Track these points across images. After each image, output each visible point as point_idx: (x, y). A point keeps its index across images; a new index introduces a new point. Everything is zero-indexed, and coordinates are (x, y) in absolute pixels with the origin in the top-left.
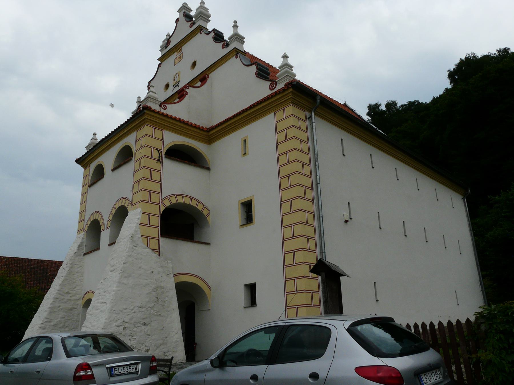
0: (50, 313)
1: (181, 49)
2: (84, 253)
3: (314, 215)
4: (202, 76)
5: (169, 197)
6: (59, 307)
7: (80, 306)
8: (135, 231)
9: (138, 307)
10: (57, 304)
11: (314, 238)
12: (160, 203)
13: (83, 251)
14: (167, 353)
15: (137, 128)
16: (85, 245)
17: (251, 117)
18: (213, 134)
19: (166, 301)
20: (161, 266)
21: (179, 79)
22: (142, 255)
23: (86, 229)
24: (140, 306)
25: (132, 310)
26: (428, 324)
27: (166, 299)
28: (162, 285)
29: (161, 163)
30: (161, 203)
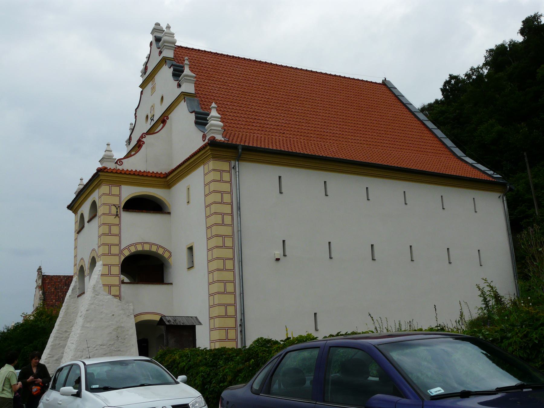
2: (78, 295)
3: (232, 195)
6: (59, 344)
8: (97, 282)
9: (99, 345)
10: (57, 342)
12: (119, 254)
13: (76, 293)
15: (98, 186)
16: (78, 287)
17: (196, 163)
19: (126, 338)
20: (122, 309)
22: (103, 301)
24: (101, 344)
25: (94, 348)
27: (126, 336)
28: (123, 325)
29: (119, 218)
30: (121, 253)
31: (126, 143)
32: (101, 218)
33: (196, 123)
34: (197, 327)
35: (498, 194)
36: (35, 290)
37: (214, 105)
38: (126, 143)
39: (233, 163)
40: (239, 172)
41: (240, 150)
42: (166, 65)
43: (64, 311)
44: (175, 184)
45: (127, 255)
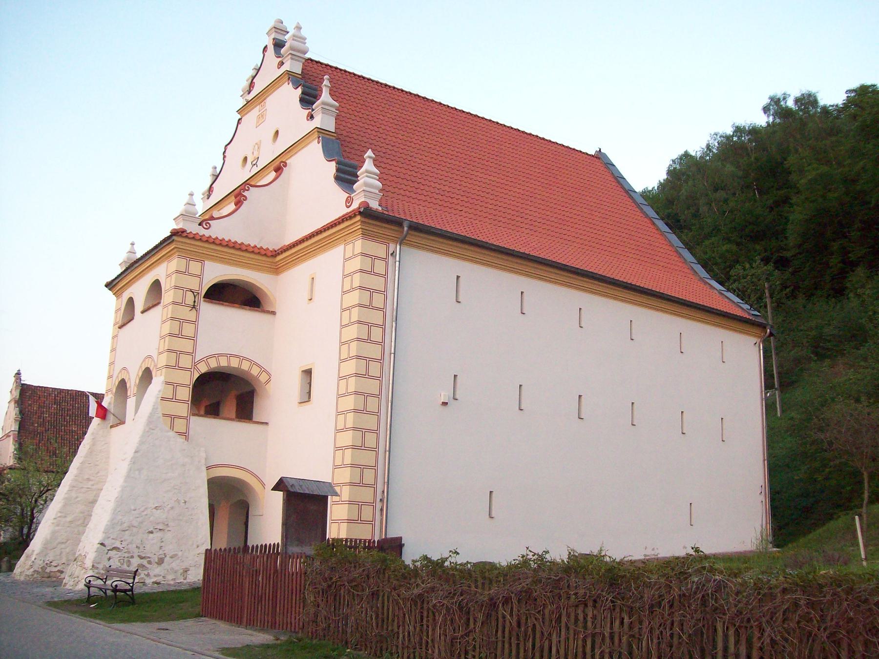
0: (65, 505)
4: (276, 163)
10: (74, 495)
14: (584, 612)
18: (279, 261)
23: (114, 390)
31: (203, 196)
32: (168, 309)
33: (337, 179)
36: (8, 405)
37: (370, 153)
38: (203, 196)
39: (392, 247)
40: (399, 262)
41: (406, 229)
42: (288, 84)
43: (88, 447)
45: (203, 372)
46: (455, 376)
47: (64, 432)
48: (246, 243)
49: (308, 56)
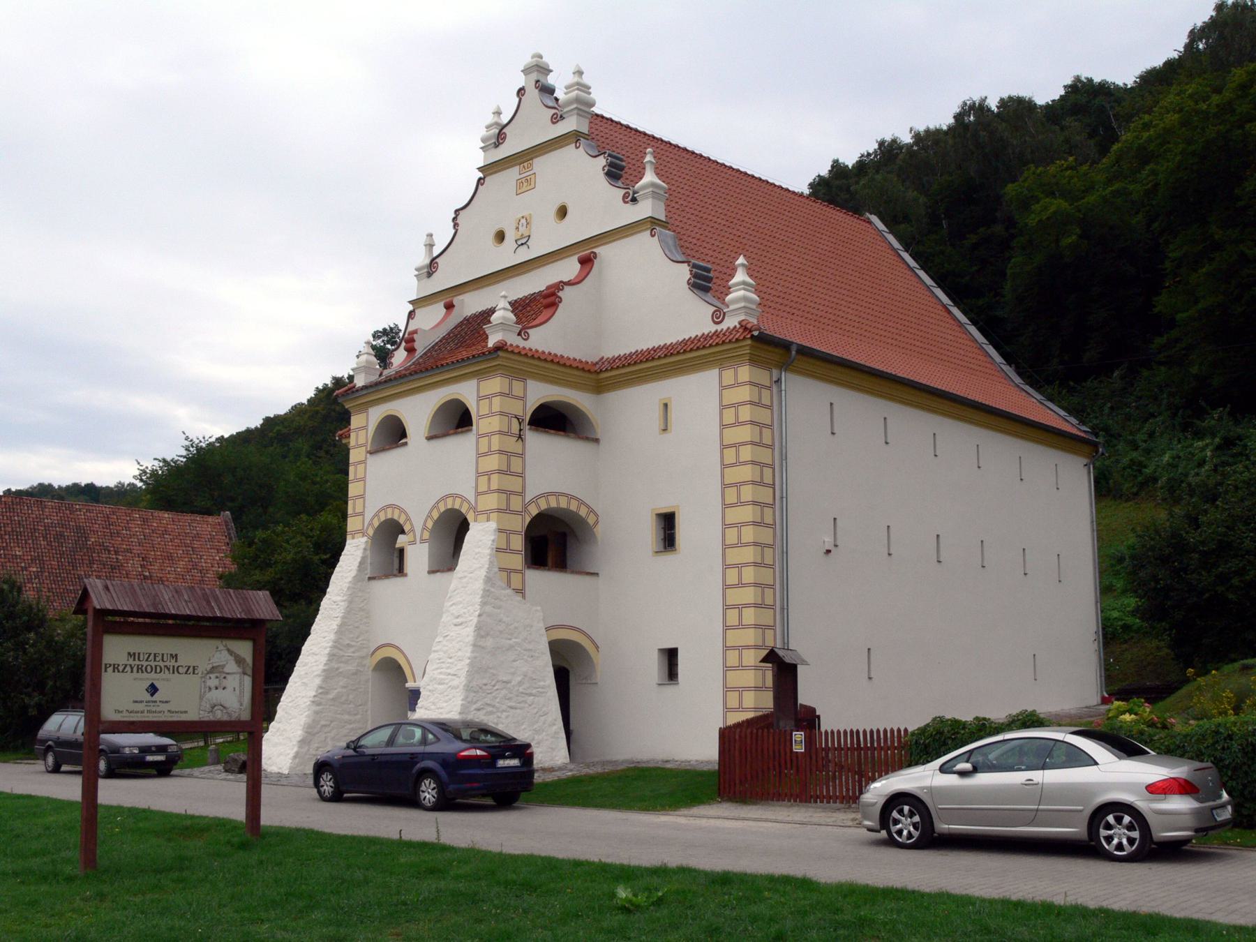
1: (531, 162)
5: (535, 500)
6: (337, 669)
7: (368, 668)
11: (772, 587)
18: (606, 378)
21: (530, 229)
22: (501, 600)
23: (371, 532)
26: (855, 730)
34: (800, 669)
35: (1085, 461)
37: (741, 260)
41: (794, 353)
44: (609, 390)
46: (835, 519)
47: (5, 558)
48: (553, 352)
49: (596, 110)
